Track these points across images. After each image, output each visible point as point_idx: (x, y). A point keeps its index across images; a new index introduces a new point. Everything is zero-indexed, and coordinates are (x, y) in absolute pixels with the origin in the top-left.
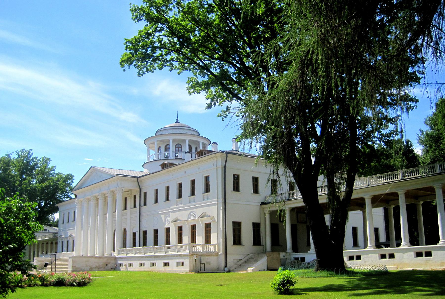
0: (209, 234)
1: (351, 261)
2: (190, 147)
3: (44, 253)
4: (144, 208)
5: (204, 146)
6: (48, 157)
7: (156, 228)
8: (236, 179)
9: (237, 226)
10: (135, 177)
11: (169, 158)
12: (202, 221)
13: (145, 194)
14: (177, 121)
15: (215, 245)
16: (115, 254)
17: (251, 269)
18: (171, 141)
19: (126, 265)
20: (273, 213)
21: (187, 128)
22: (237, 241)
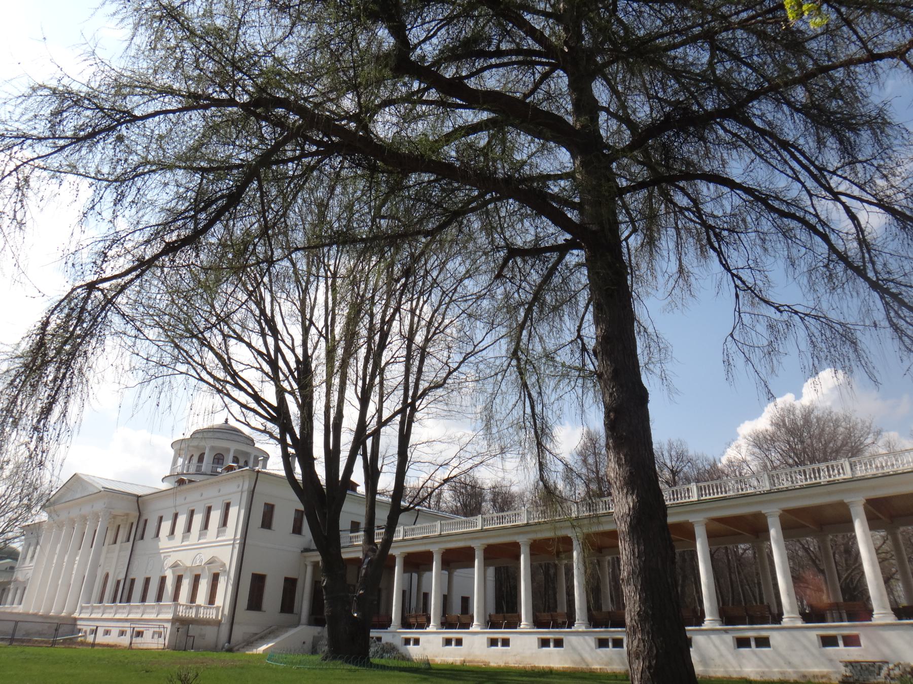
1: (544, 649)
8: (269, 510)
9: (258, 581)
12: (209, 569)
13: (146, 521)
15: (218, 608)
16: (76, 615)
19: (85, 632)
22: (255, 603)
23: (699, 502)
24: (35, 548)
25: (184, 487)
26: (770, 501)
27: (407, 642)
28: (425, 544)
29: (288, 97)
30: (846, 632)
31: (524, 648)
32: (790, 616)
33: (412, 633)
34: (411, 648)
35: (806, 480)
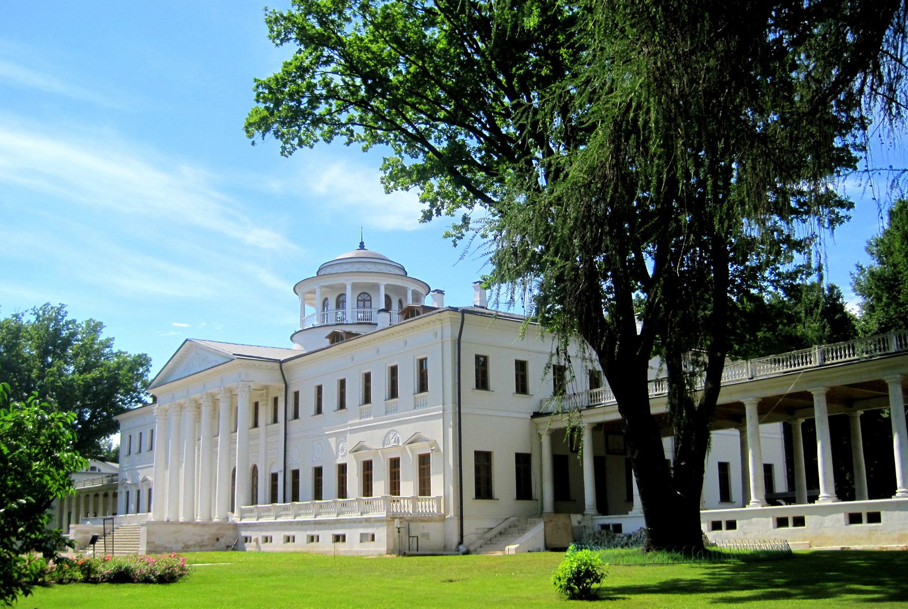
0: (426, 477)
2: (388, 299)
4: (294, 424)
5: (417, 297)
6: (98, 320)
7: (318, 465)
8: (482, 364)
9: (484, 460)
10: (275, 361)
11: (345, 322)
12: (412, 450)
13: (297, 394)
14: (362, 246)
15: (438, 499)
16: (235, 518)
17: (512, 548)
18: (349, 288)
19: (257, 540)
20: (556, 435)
21: (381, 260)
22: (484, 490)
24: (232, 442)
29: (707, 346)
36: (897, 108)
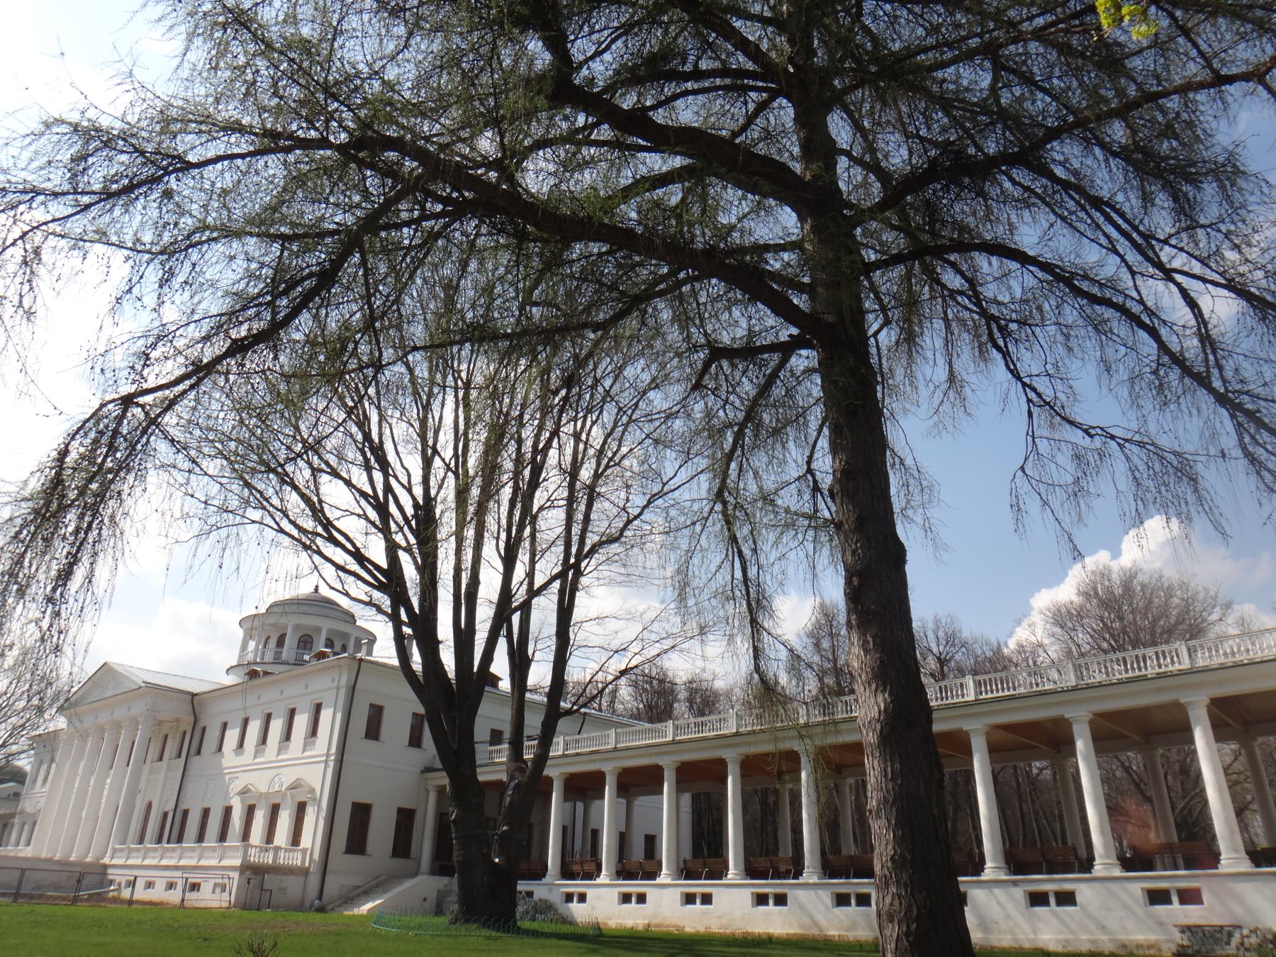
1: (761, 908)
3: (211, 841)
8: (376, 713)
9: (361, 813)
12: (292, 797)
13: (204, 729)
15: (304, 851)
16: (106, 860)
19: (119, 884)
22: (357, 844)
23: (977, 702)
24: (49, 767)
25: (257, 682)
26: (1077, 702)
27: (569, 898)
28: (594, 761)
30: (1183, 884)
31: (732, 906)
32: (1104, 862)
33: (575, 886)
34: (575, 907)
35: (1127, 671)
36: (748, 352)
